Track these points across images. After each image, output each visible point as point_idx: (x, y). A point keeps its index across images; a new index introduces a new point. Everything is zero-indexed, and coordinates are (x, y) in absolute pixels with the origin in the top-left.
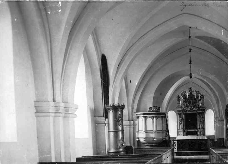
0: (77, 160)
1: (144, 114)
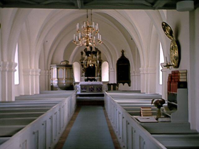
0: (16, 100)
1: (57, 66)
